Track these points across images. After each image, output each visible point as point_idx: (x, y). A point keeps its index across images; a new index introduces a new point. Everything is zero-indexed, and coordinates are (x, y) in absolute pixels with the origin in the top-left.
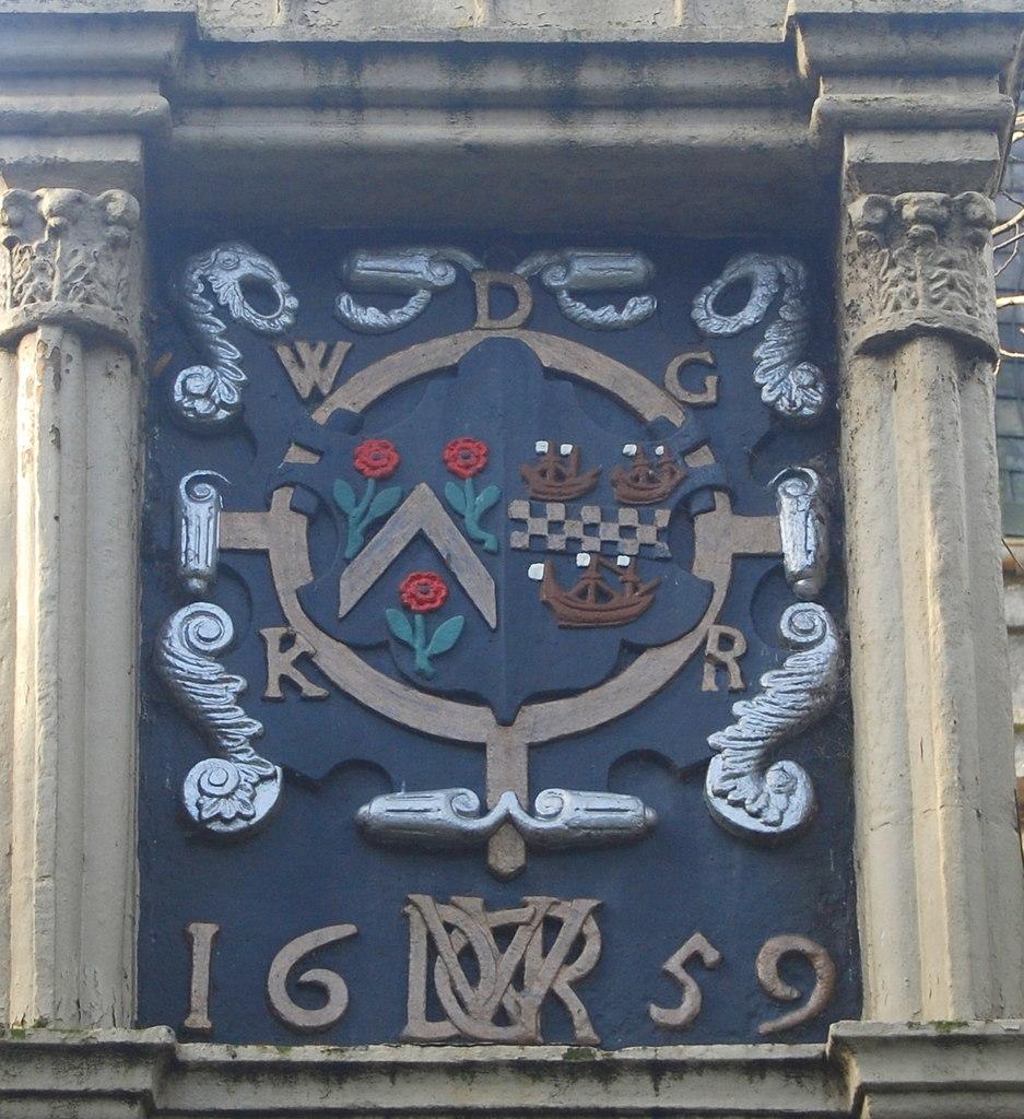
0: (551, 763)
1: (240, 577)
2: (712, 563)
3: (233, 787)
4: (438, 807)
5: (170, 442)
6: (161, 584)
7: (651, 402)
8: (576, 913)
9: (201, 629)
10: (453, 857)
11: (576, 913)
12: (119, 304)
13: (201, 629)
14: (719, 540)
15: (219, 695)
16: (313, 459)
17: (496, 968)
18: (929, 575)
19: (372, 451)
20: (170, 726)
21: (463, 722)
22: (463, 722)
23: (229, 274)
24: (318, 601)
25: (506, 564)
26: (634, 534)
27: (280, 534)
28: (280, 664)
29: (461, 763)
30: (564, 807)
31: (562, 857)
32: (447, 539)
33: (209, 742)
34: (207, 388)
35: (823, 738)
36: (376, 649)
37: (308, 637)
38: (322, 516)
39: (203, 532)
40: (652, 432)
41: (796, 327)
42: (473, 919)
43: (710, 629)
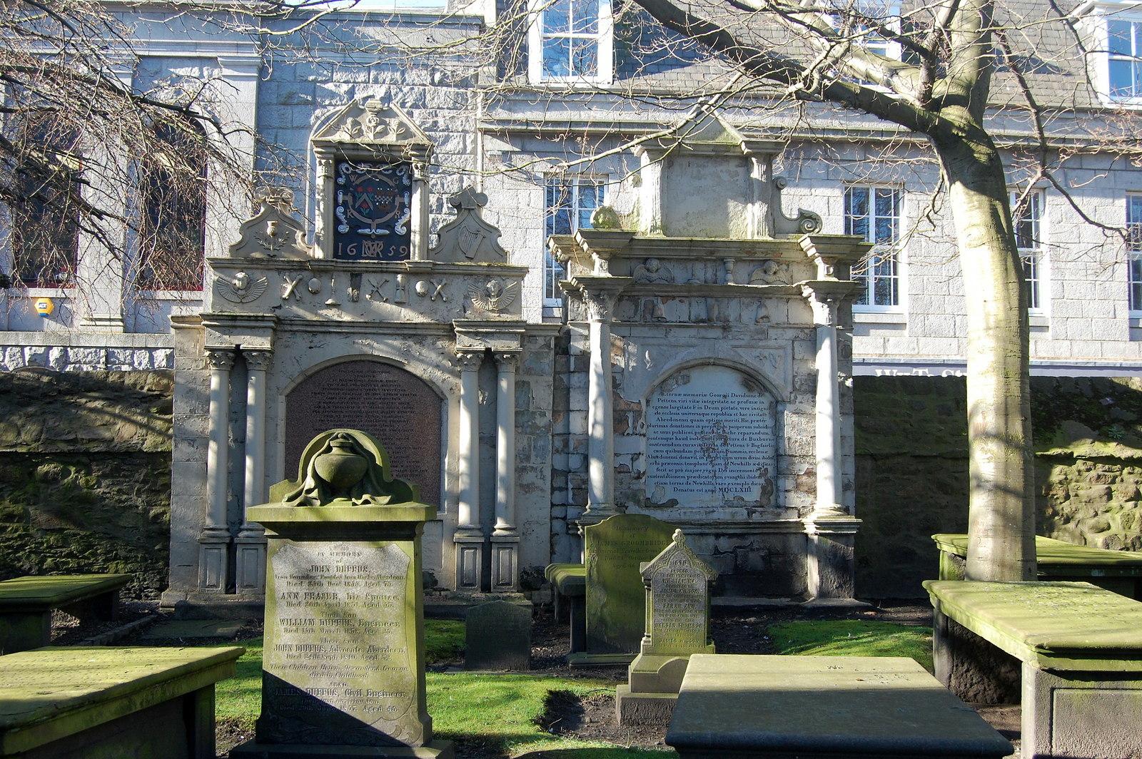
0: (379, 226)
1: (345, 204)
2: (397, 204)
3: (344, 229)
4: (367, 231)
5: (337, 187)
6: (336, 204)
7: (391, 183)
8: (381, 243)
9: (341, 209)
10: (368, 237)
11: (381, 243)
12: (332, 174)
13: (341, 209)
14: (398, 200)
15: (342, 217)
16: (286, 295)
17: (372, 249)
18: (71, 448)
19: (360, 189)
20: (337, 222)
21: (369, 221)
22: (369, 221)
23: (343, 167)
24: (353, 207)
25: (374, 203)
26: (388, 200)
27: (349, 199)
28: (349, 214)
29: (369, 226)
30: (380, 232)
31: (380, 237)
32: (367, 200)
33: (341, 223)
34: (341, 181)
35: (408, 224)
36: (360, 212)
37: (352, 211)
38: (354, 197)
39: (341, 198)
40: (390, 187)
41: (139, 446)
42: (370, 243)
43: (396, 211)
